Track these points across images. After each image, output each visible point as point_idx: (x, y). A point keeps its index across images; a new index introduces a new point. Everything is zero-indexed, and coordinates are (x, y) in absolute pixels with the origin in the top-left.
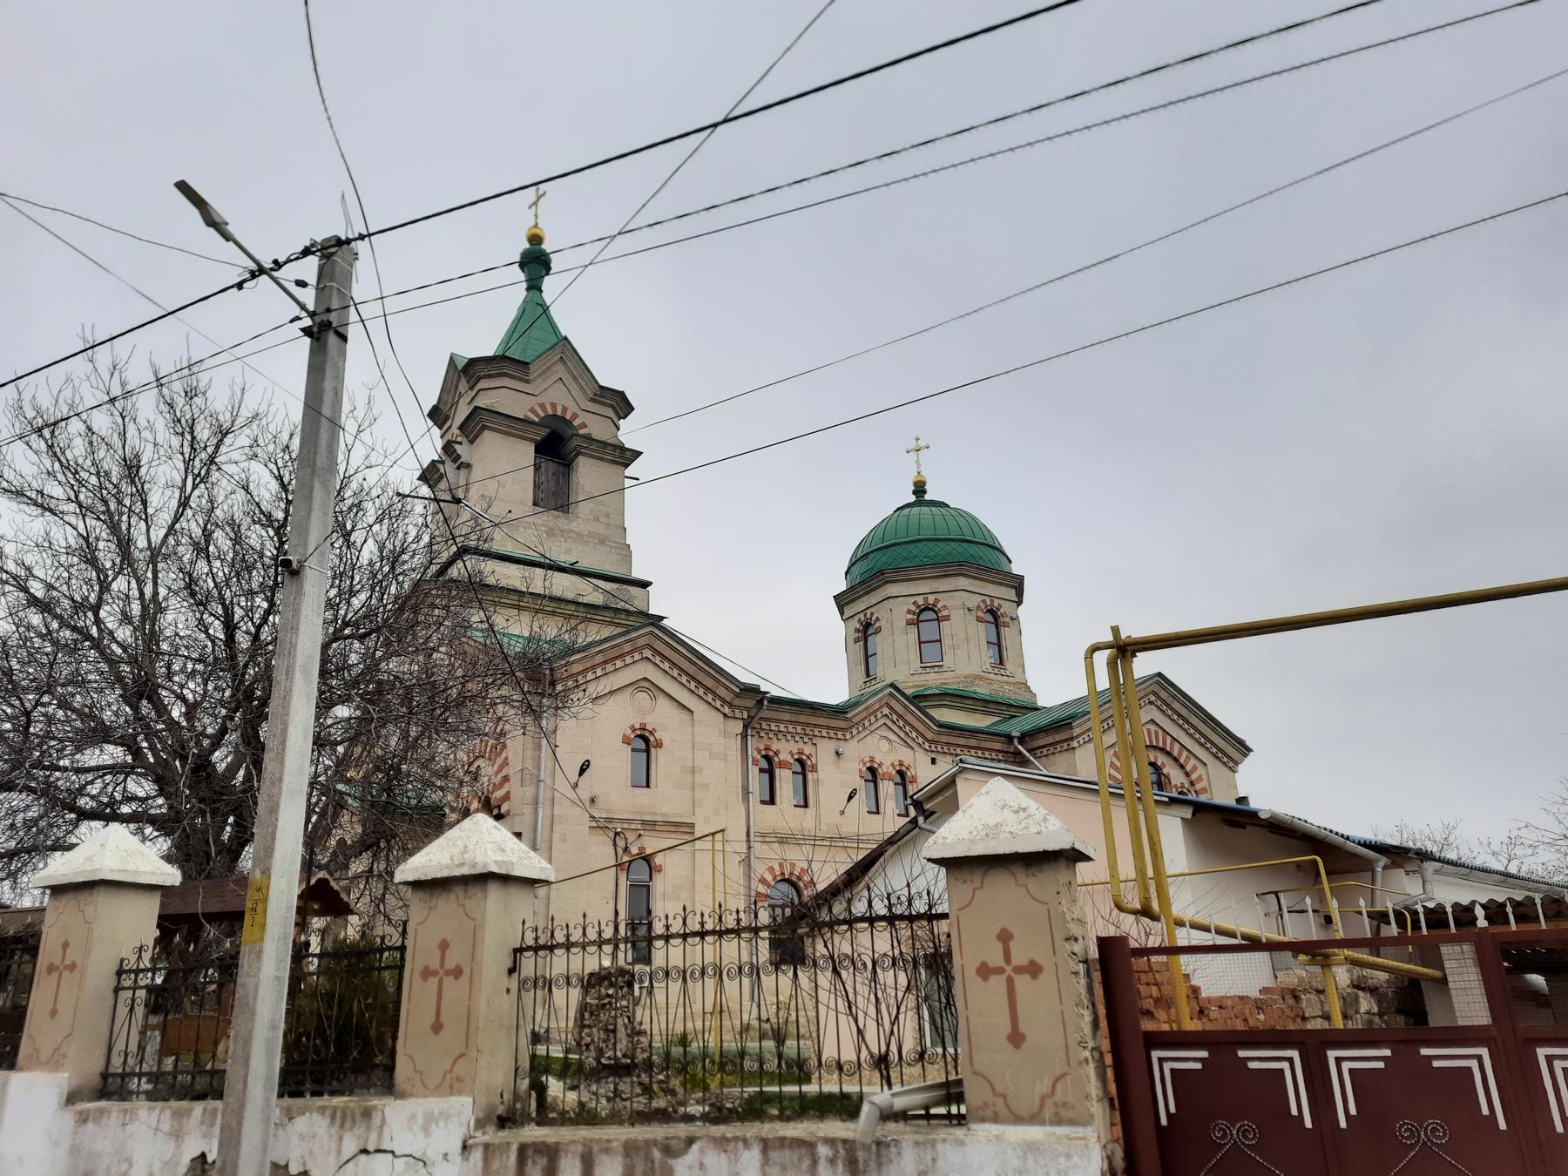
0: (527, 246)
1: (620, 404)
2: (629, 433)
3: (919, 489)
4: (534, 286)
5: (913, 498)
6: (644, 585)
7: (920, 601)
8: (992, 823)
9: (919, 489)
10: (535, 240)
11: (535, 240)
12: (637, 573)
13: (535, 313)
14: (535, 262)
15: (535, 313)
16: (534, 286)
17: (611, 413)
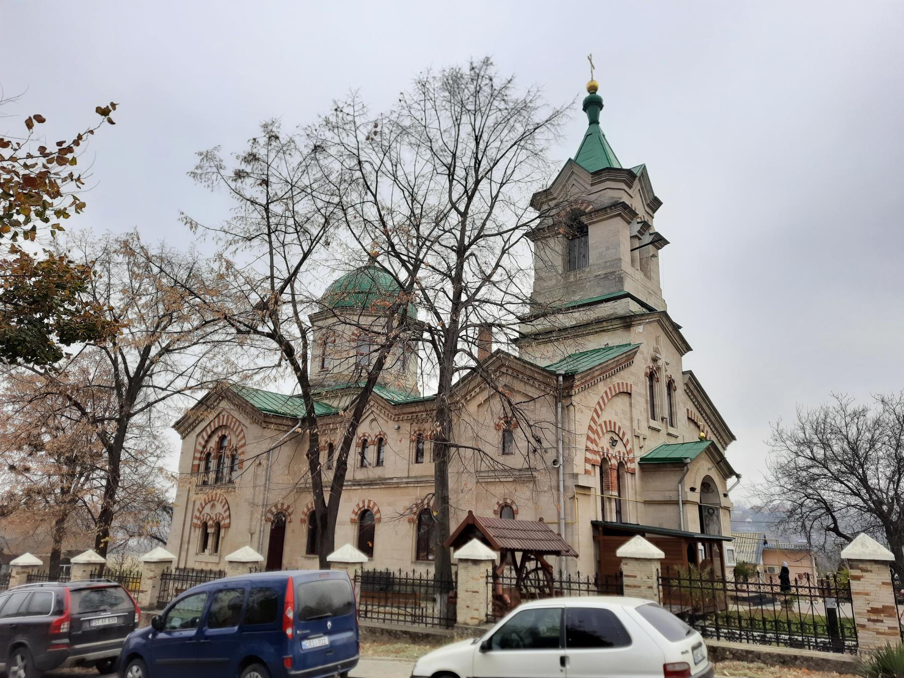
0: (588, 94)
4: (594, 121)
10: (593, 89)
11: (593, 89)
13: (594, 137)
14: (593, 105)
15: (594, 137)
16: (594, 121)
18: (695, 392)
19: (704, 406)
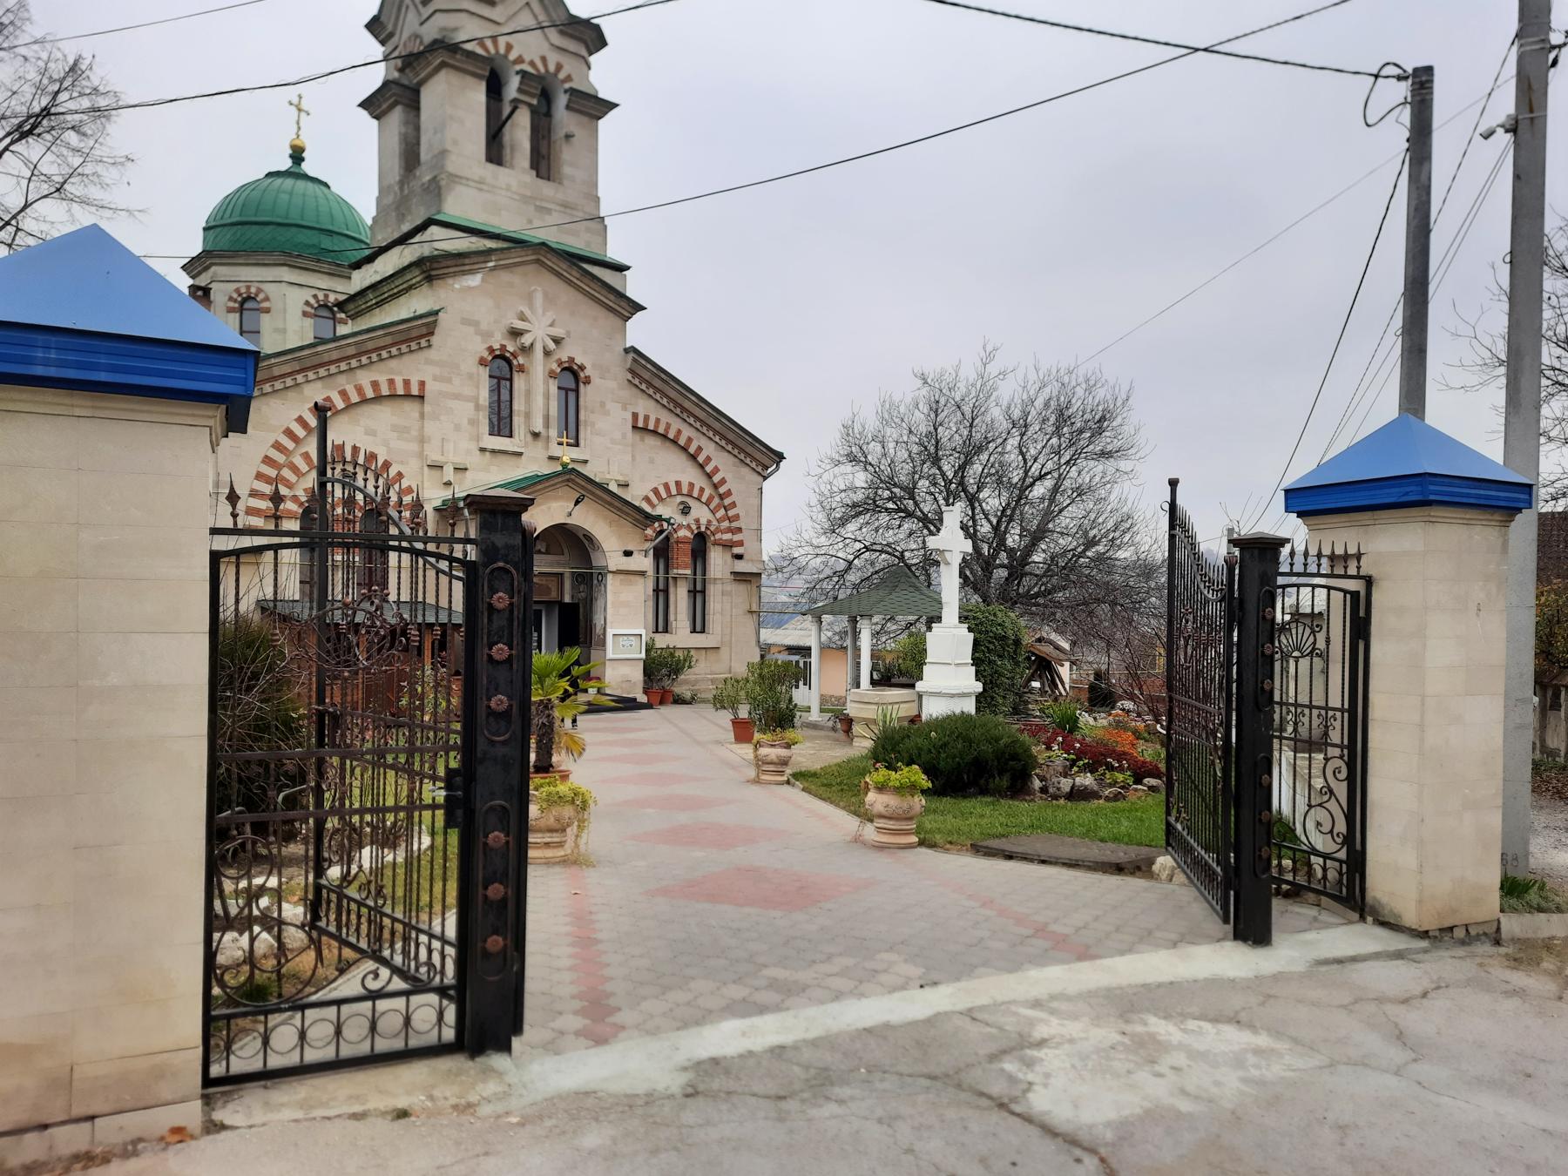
1: (589, 36)
2: (602, 75)
3: (297, 155)
5: (285, 164)
6: (620, 268)
7: (321, 296)
8: (578, 361)
9: (297, 155)
12: (614, 253)
17: (584, 52)
18: (657, 383)
19: (687, 404)
